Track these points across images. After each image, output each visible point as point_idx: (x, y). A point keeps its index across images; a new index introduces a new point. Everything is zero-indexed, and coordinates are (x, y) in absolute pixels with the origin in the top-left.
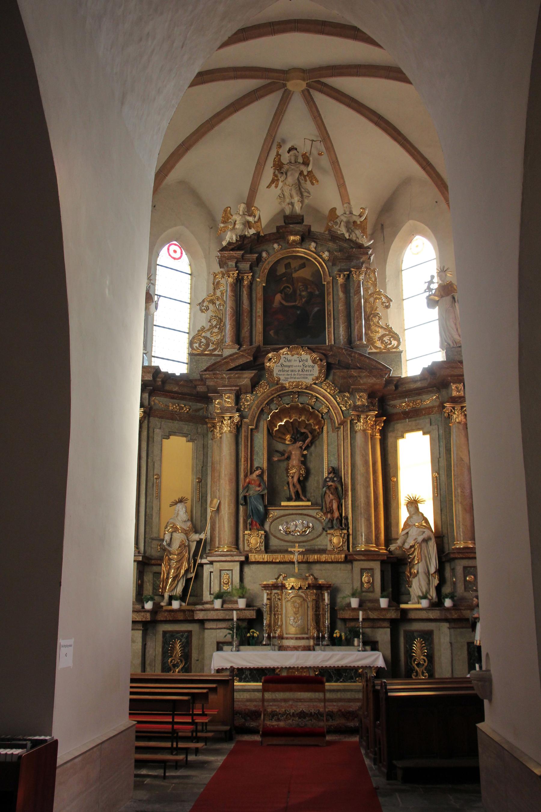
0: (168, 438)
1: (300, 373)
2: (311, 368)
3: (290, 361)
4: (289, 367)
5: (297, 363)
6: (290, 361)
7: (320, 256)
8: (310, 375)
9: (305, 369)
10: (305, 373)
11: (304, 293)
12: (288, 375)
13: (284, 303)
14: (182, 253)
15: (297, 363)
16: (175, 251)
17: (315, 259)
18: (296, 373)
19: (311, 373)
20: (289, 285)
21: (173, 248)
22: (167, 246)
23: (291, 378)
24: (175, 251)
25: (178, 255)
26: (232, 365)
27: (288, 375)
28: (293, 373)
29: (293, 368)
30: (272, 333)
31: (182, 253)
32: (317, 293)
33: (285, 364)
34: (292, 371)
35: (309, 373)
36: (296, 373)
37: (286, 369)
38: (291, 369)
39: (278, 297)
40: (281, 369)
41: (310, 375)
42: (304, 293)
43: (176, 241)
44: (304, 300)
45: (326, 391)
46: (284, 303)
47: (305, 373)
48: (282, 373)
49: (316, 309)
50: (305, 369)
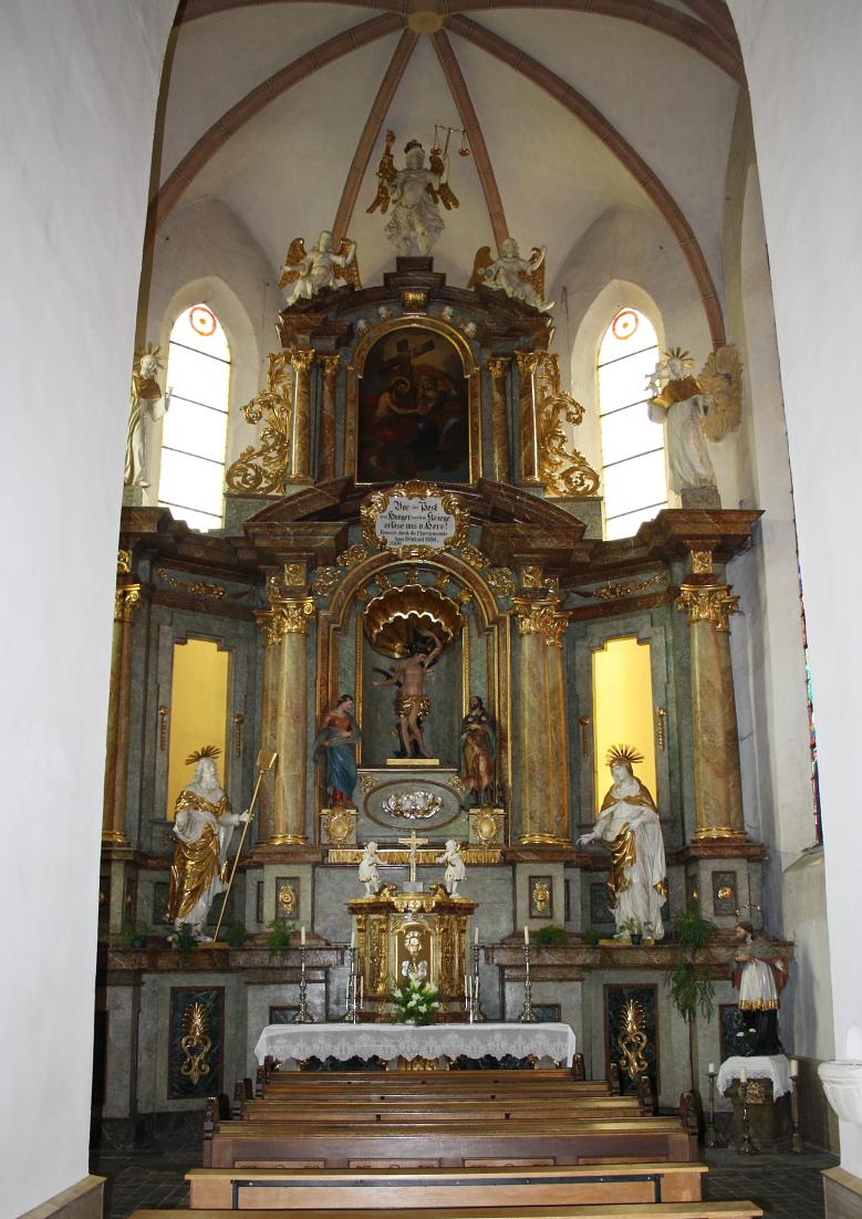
0: (183, 642)
1: (423, 530)
2: (442, 523)
3: (405, 508)
4: (404, 518)
5: (418, 513)
6: (405, 508)
7: (461, 331)
8: (441, 534)
9: (433, 523)
10: (432, 531)
11: (430, 394)
12: (400, 533)
13: (394, 408)
14: (214, 325)
15: (418, 513)
16: (203, 321)
17: (451, 335)
18: (415, 530)
19: (442, 531)
20: (403, 378)
21: (199, 315)
22: (189, 310)
23: (407, 539)
24: (203, 321)
25: (208, 328)
26: (304, 512)
27: (400, 533)
28: (410, 530)
29: (411, 522)
30: (373, 460)
31: (214, 325)
32: (454, 393)
33: (396, 513)
34: (409, 526)
35: (440, 531)
36: (415, 530)
37: (399, 522)
38: (407, 522)
39: (385, 399)
40: (389, 522)
41: (441, 534)
42: (430, 394)
43: (204, 302)
44: (430, 405)
45: (469, 564)
46: (394, 408)
47: (432, 531)
48: (390, 530)
49: (452, 422)
50: (433, 523)
